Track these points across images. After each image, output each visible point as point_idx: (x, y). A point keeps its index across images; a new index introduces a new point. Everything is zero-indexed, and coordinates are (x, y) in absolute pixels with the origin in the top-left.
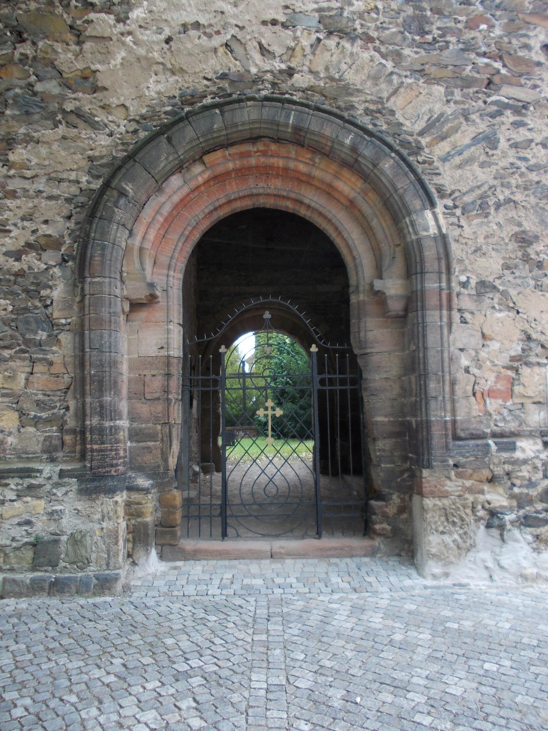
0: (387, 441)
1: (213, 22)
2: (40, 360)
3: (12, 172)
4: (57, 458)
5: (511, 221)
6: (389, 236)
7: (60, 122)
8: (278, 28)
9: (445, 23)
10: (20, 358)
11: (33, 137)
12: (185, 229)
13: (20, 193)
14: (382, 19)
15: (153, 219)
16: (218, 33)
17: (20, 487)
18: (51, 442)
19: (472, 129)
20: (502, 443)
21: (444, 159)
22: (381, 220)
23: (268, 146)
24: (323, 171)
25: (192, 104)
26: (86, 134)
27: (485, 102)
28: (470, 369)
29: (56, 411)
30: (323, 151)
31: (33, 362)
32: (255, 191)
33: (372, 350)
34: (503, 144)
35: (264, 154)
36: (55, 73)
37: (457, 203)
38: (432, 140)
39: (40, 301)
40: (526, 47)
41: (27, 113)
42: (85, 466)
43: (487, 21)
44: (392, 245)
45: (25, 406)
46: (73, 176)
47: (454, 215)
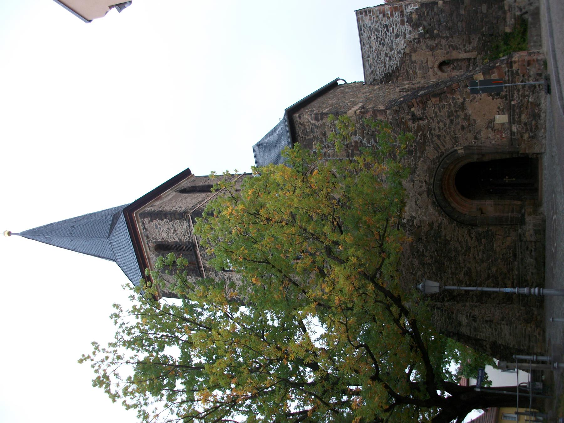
21: (444, 147)
34: (439, 133)
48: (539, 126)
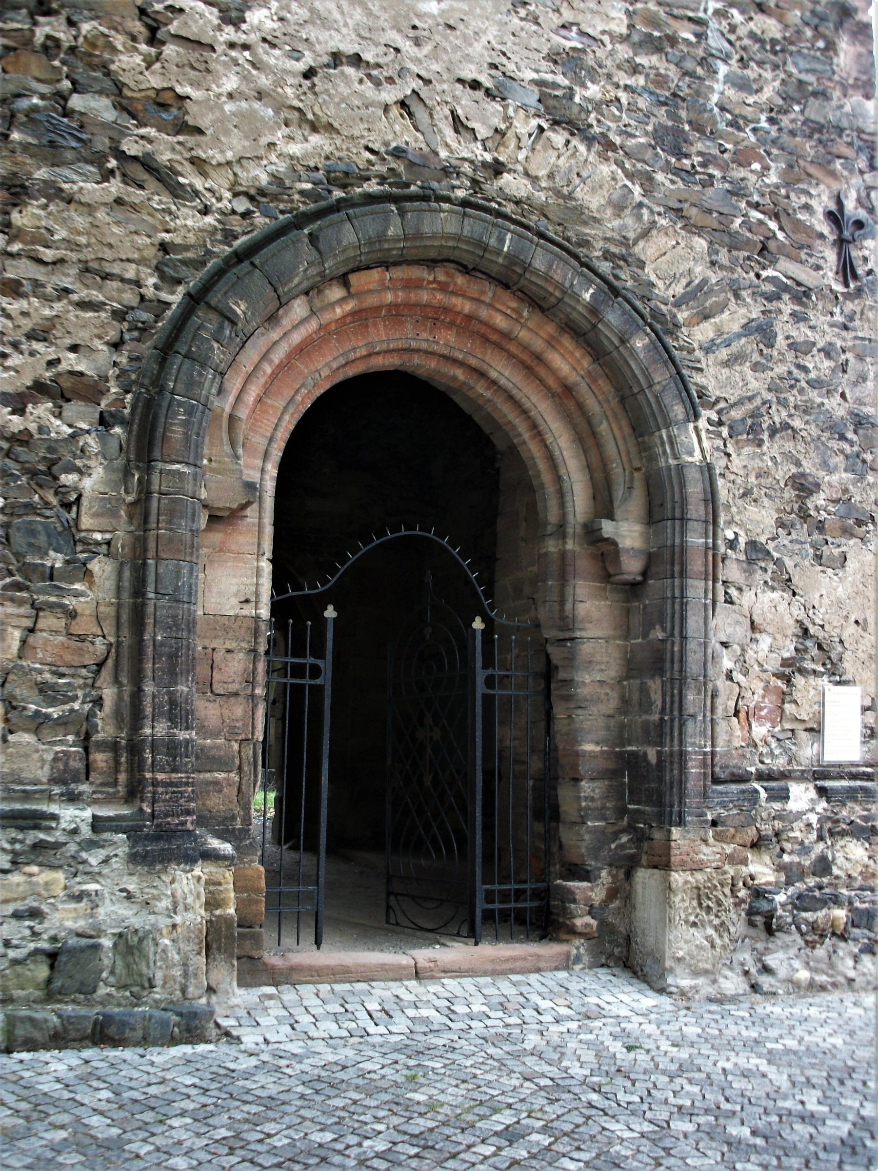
0: (598, 784)
1: (381, 61)
2: (51, 606)
3: (16, 247)
4: (81, 794)
5: (790, 458)
6: (623, 454)
7: (112, 172)
8: (480, 94)
9: (708, 147)
10: (12, 600)
11: (61, 190)
12: (297, 391)
13: (27, 287)
14: (625, 119)
15: (257, 367)
16: (390, 80)
17: (18, 846)
18: (66, 764)
19: (743, 311)
20: (773, 789)
21: (708, 349)
22: (614, 426)
23: (451, 276)
24: (533, 332)
25: (344, 187)
26: (160, 202)
27: (758, 276)
28: (734, 674)
29: (76, 706)
30: (541, 303)
31: (38, 609)
32: (414, 344)
33: (583, 634)
34: (781, 342)
35: (443, 287)
36: (108, 84)
37: (723, 419)
38: (692, 317)
39: (56, 493)
40: (807, 207)
41: (52, 144)
42: (141, 810)
43: (760, 159)
44: (627, 466)
45: (18, 692)
46: (130, 272)
47: (719, 435)
48: (821, 952)
